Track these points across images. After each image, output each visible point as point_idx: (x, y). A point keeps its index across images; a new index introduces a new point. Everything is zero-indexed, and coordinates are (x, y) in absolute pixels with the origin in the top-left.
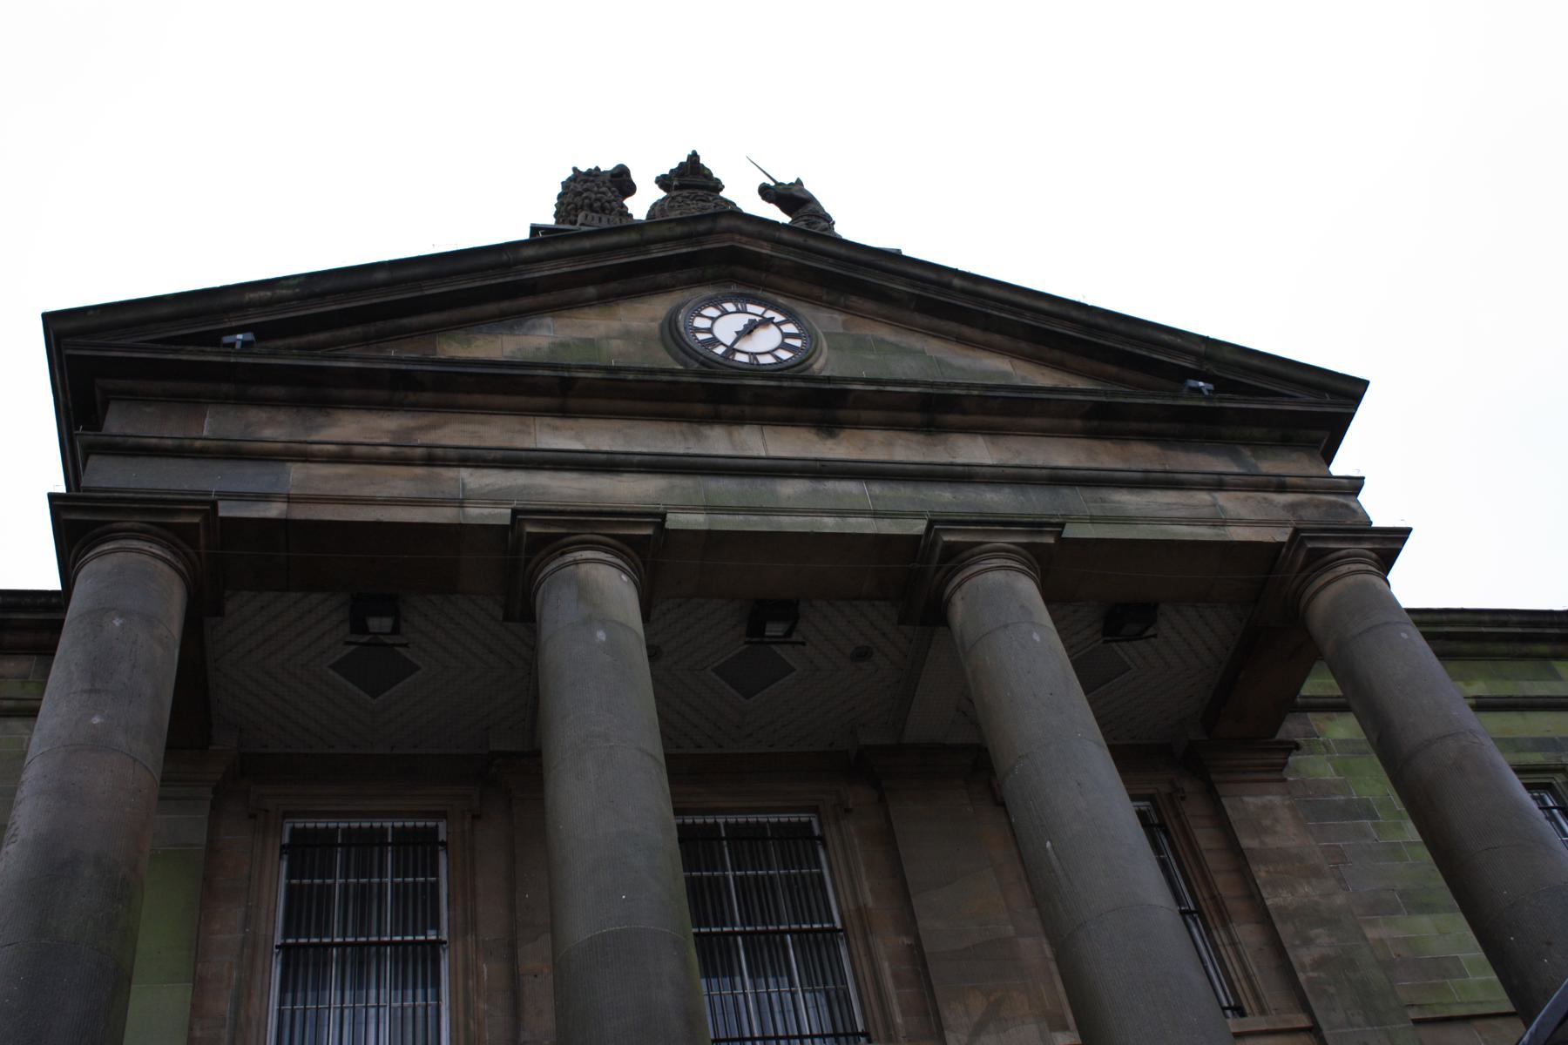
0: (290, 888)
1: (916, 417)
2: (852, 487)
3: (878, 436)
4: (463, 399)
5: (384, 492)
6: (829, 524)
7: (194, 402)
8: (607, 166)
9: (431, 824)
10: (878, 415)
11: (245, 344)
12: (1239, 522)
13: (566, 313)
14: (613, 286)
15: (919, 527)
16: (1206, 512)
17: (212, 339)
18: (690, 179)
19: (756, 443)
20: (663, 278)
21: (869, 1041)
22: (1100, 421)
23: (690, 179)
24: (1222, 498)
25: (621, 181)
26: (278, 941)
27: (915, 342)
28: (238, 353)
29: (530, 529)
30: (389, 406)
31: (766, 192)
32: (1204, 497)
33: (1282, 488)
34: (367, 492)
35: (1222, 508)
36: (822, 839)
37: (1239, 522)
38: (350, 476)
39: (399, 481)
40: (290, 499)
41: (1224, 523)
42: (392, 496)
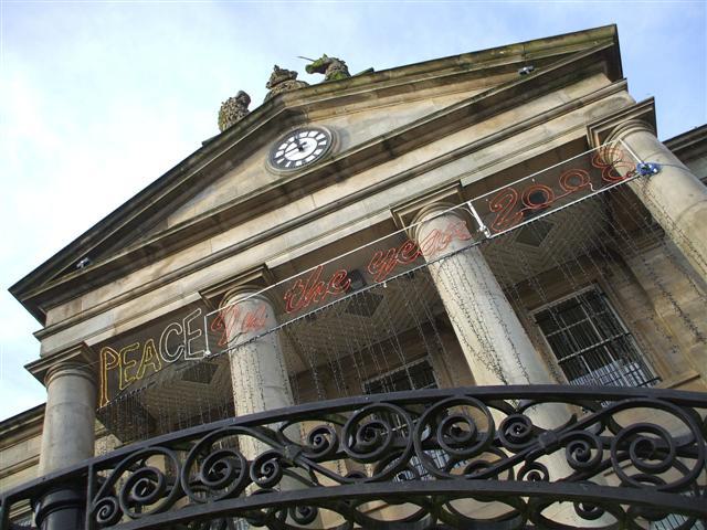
0: (548, 338)
1: (385, 155)
2: (356, 206)
3: (369, 172)
4: (177, 245)
5: (150, 305)
7: (124, 274)
8: (234, 95)
9: (422, 360)
10: (366, 163)
11: (85, 264)
12: (560, 135)
13: (213, 187)
14: (238, 156)
15: (388, 215)
16: (540, 138)
17: (74, 268)
18: (282, 77)
19: (308, 204)
20: (261, 140)
21: (661, 381)
22: (478, 111)
23: (282, 77)
24: (548, 125)
25: (243, 99)
26: (557, 362)
27: (383, 113)
28: (528, 76)
29: (208, 297)
30: (150, 263)
31: (311, 69)
32: (539, 129)
33: (581, 105)
34: (144, 308)
35: (550, 132)
36: (604, 294)
37: (560, 135)
38: (136, 305)
39: (156, 297)
40: (182, 296)
41: (552, 138)
42: (156, 305)
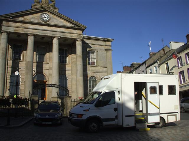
6: (46, 35)
32: (72, 34)
41: (72, 37)
